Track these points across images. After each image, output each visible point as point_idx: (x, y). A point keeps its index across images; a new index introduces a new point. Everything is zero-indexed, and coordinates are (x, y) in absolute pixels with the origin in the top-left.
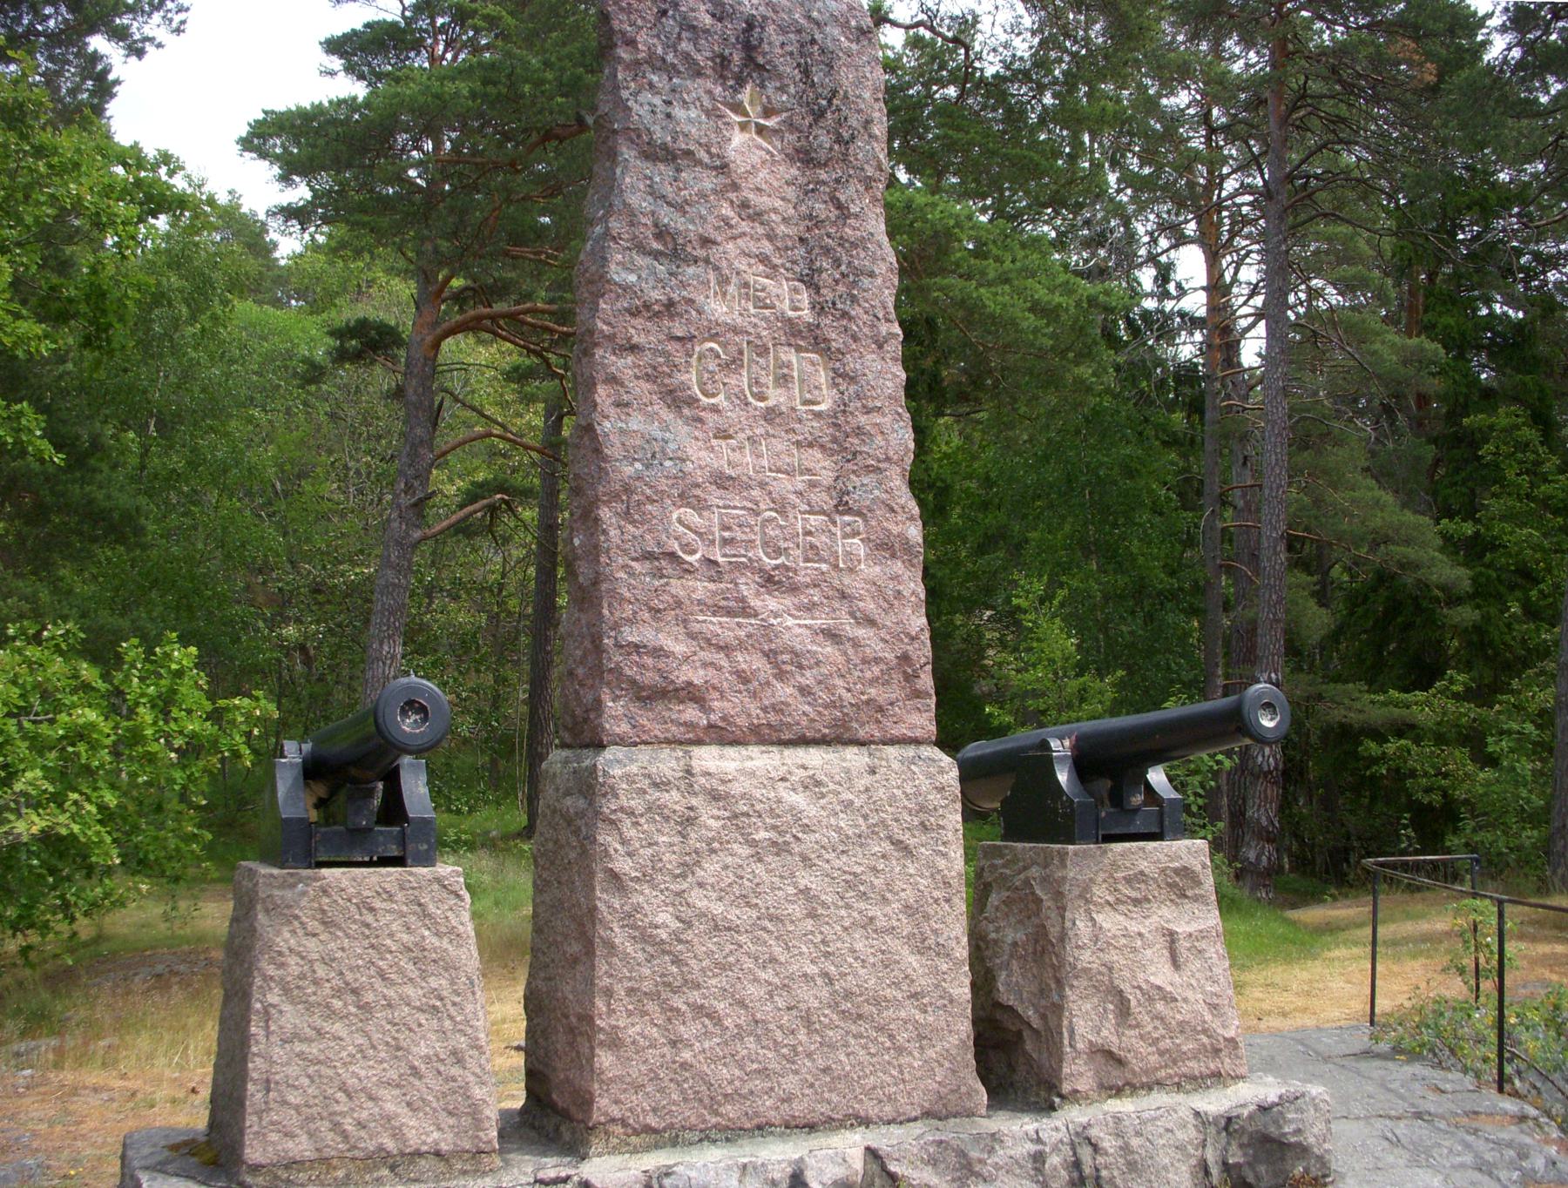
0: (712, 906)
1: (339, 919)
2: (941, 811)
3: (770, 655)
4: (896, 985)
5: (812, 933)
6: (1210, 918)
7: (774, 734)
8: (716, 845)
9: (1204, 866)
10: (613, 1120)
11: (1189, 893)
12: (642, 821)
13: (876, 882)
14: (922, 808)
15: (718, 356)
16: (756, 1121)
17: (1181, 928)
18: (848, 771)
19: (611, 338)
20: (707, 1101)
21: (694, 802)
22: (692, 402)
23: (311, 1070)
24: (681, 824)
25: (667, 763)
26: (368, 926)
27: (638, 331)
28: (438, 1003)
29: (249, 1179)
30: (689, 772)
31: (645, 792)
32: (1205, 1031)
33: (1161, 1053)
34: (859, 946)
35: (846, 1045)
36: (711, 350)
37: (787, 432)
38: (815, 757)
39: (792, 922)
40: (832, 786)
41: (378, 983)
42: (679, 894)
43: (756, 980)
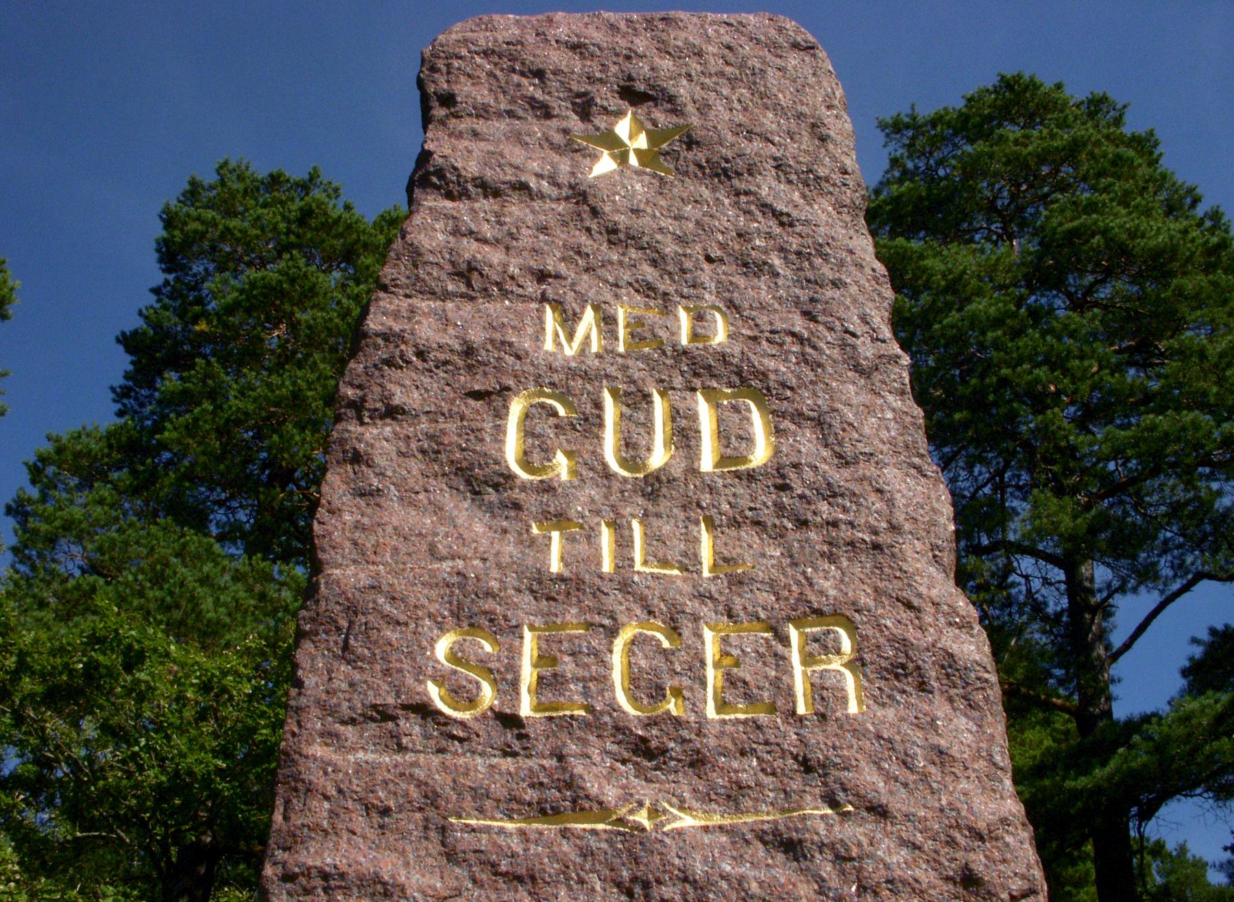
15: (555, 414)
19: (358, 406)
27: (406, 390)
36: (543, 406)
37: (684, 508)
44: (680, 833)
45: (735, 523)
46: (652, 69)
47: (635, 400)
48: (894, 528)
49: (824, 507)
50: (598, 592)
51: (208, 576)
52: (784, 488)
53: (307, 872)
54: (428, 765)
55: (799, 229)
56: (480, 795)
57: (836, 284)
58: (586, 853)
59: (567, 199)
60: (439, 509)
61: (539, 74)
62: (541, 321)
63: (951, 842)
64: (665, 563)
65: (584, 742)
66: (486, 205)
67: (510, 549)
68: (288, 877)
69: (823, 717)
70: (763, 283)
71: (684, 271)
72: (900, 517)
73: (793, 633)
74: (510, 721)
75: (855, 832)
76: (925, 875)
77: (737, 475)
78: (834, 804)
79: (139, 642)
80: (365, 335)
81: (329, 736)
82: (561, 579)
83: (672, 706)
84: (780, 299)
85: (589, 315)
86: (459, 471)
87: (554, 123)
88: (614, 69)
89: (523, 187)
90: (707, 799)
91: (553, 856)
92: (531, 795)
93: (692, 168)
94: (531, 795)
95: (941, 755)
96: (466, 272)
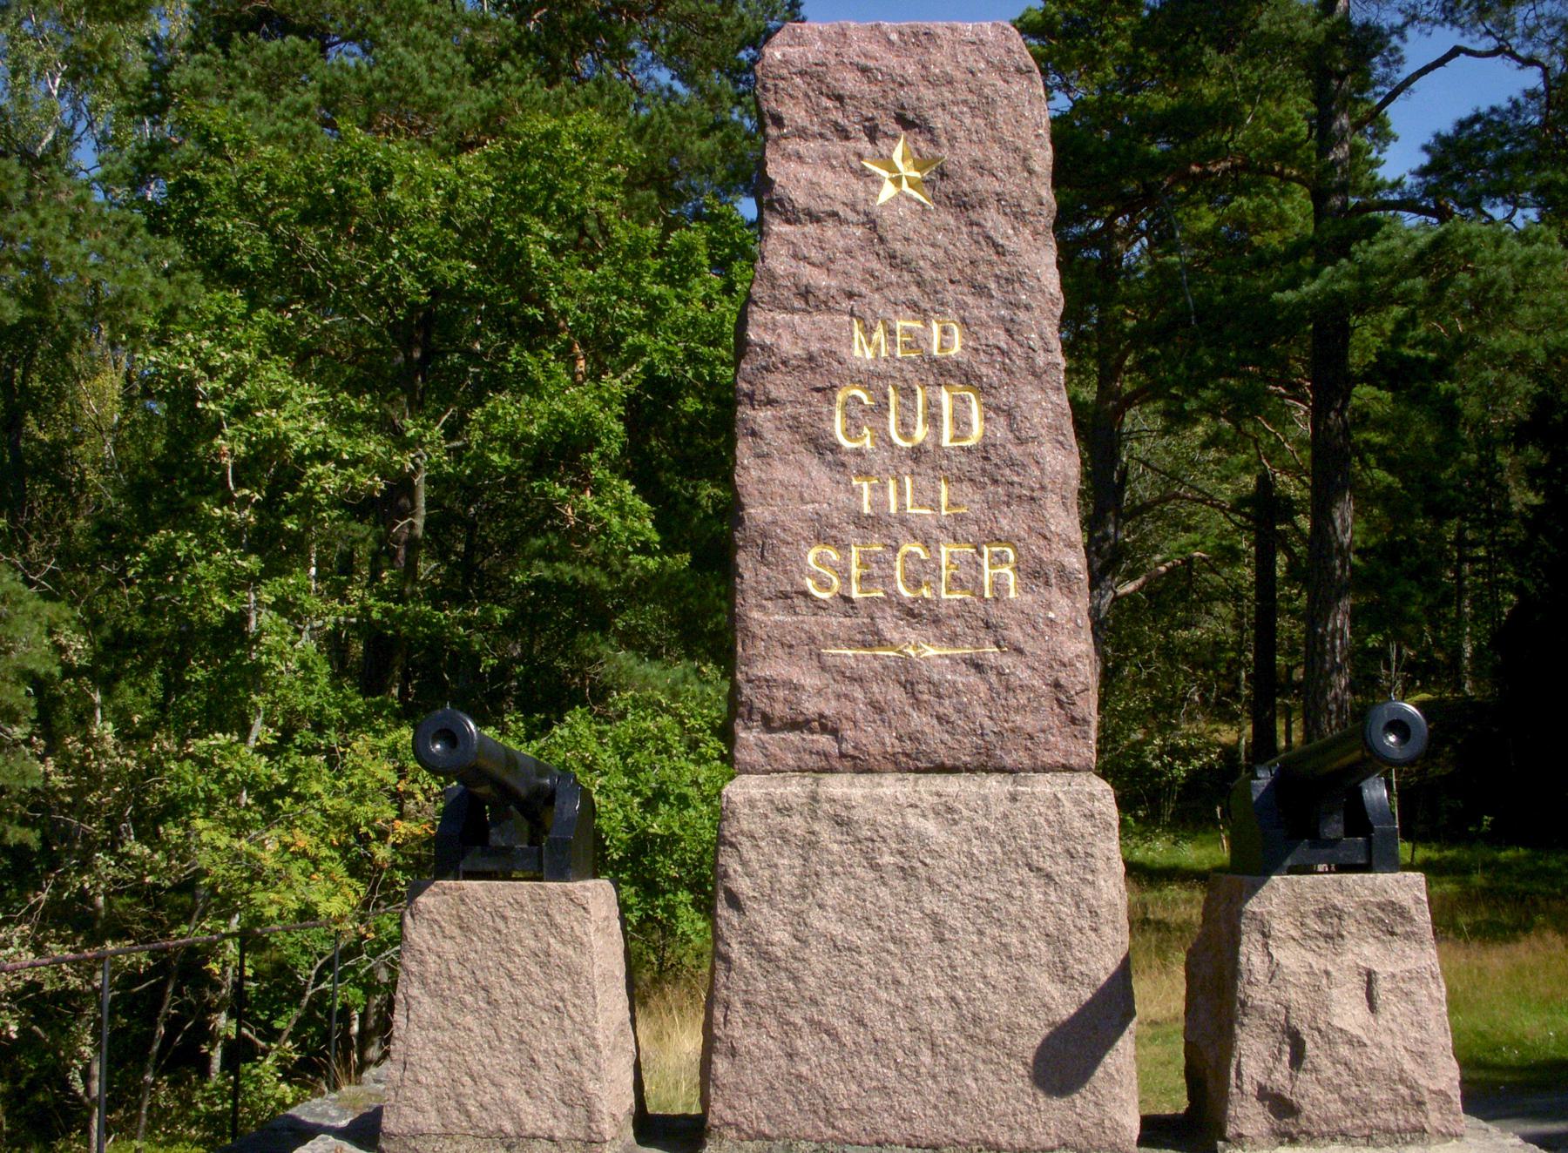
0: (831, 926)
1: (474, 925)
2: (1090, 839)
3: (909, 686)
4: (1034, 1013)
5: (940, 957)
6: (1426, 957)
7: (917, 762)
8: (838, 869)
9: (1417, 901)
10: (728, 1124)
11: (1398, 930)
12: (763, 844)
13: (1012, 909)
14: (1066, 836)
15: (861, 403)
16: (875, 1137)
17: (1383, 969)
18: (985, 798)
19: (751, 396)
20: (822, 1113)
21: (816, 827)
22: (836, 448)
23: (442, 1055)
24: (802, 848)
25: (794, 789)
26: (499, 932)
27: (777, 385)
28: (560, 1004)
29: (384, 1145)
30: (814, 798)
31: (766, 816)
32: (1402, 1081)
33: (1345, 1101)
34: (991, 971)
35: (974, 1069)
36: (854, 397)
37: (933, 469)
38: (952, 785)
39: (917, 945)
40: (966, 813)
41: (506, 983)
42: (798, 914)
43: (877, 1000)
44: (927, 659)
45: (959, 480)
46: (918, 99)
48: (1043, 488)
49: (1007, 472)
51: (416, 37)
52: (987, 459)
53: (759, 679)
54: (810, 622)
55: (1008, 258)
56: (834, 638)
57: (1028, 308)
58: (885, 667)
59: (863, 224)
60: (801, 467)
61: (840, 98)
62: (852, 332)
63: (1051, 667)
64: (921, 506)
65: (883, 610)
66: (811, 229)
67: (842, 496)
68: (749, 681)
69: (997, 599)
70: (983, 302)
71: (936, 292)
72: (1046, 481)
73: (986, 550)
74: (847, 600)
77: (962, 448)
78: (999, 646)
79: (387, 164)
80: (748, 343)
81: (762, 608)
82: (869, 516)
83: (926, 592)
84: (992, 318)
85: (880, 328)
86: (811, 440)
87: (851, 144)
88: (891, 95)
89: (834, 214)
90: (940, 640)
91: (870, 669)
92: (859, 637)
93: (944, 199)
94: (859, 637)
96: (805, 293)
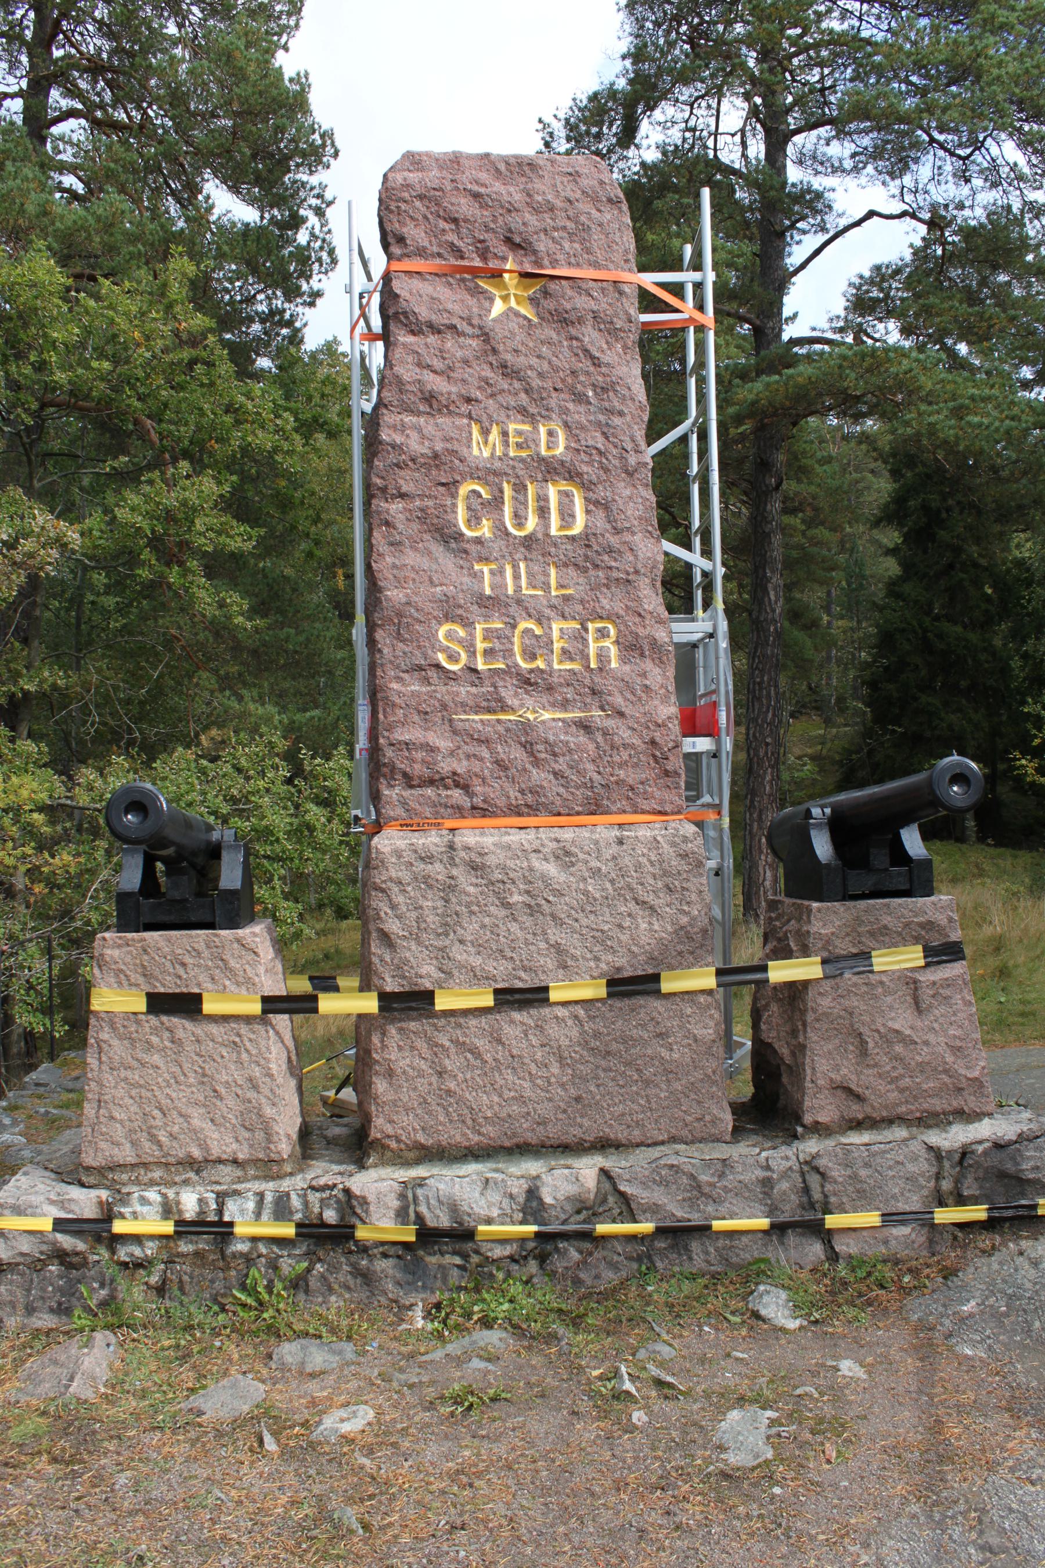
19: (384, 490)
45: (566, 565)
47: (520, 488)
48: (637, 572)
49: (606, 558)
50: (507, 605)
52: (588, 546)
58: (508, 730)
64: (534, 587)
66: (432, 339)
70: (582, 409)
72: (639, 566)
75: (610, 723)
76: (636, 741)
81: (399, 679)
86: (437, 530)
89: (453, 327)
90: (553, 705)
94: (484, 704)
95: (647, 688)
96: (429, 398)
